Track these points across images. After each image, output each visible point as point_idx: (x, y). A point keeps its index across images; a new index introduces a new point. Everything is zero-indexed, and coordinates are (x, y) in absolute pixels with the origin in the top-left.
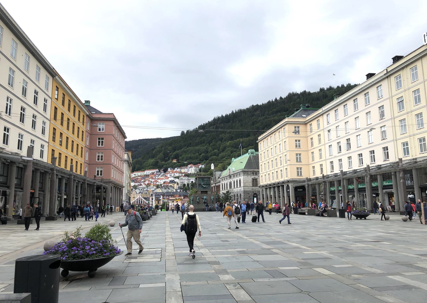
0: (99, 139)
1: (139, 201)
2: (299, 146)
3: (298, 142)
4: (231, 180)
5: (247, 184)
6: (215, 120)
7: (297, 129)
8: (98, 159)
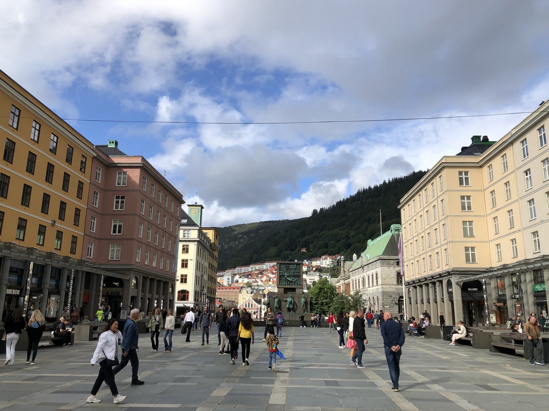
0: (118, 198)
1: (249, 304)
2: (469, 208)
3: (466, 201)
4: (365, 274)
5: (388, 281)
6: (359, 193)
7: (464, 176)
8: (114, 232)
